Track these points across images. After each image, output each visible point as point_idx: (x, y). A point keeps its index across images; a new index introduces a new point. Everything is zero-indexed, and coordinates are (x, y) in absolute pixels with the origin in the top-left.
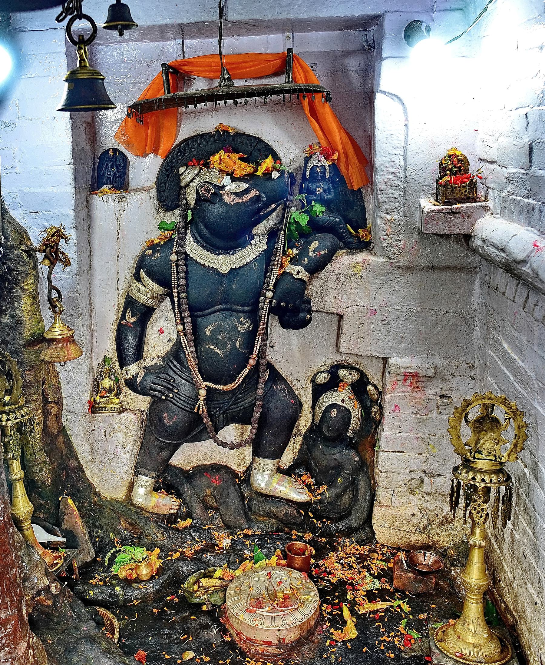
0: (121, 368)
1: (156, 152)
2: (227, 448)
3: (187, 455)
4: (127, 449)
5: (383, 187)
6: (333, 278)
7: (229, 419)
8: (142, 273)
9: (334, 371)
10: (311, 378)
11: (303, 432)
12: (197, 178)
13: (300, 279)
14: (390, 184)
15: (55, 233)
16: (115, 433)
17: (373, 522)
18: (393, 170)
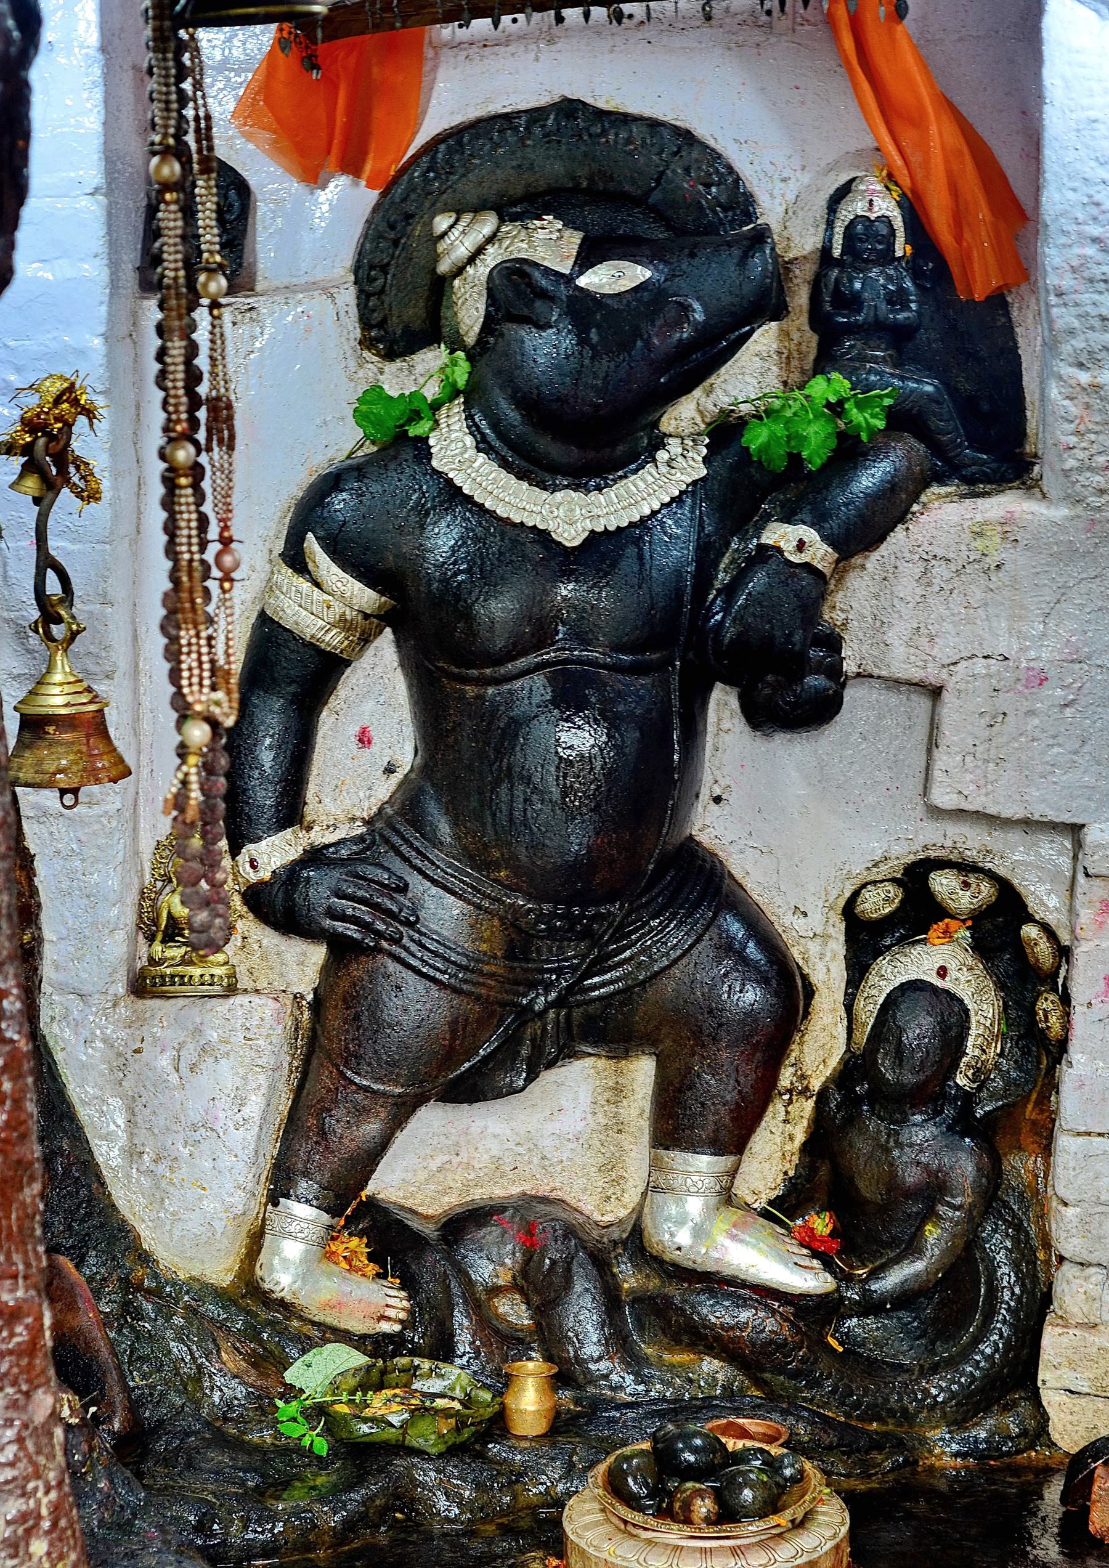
0: (235, 851)
1: (352, 166)
2: (564, 1135)
3: (434, 1165)
4: (246, 1111)
5: (1067, 282)
6: (911, 570)
7: (575, 1030)
8: (311, 543)
9: (915, 877)
10: (842, 902)
11: (816, 1085)
12: (490, 250)
13: (807, 567)
14: (1086, 274)
15: (63, 393)
16: (211, 1060)
17: (1040, 1377)
18: (1096, 231)
